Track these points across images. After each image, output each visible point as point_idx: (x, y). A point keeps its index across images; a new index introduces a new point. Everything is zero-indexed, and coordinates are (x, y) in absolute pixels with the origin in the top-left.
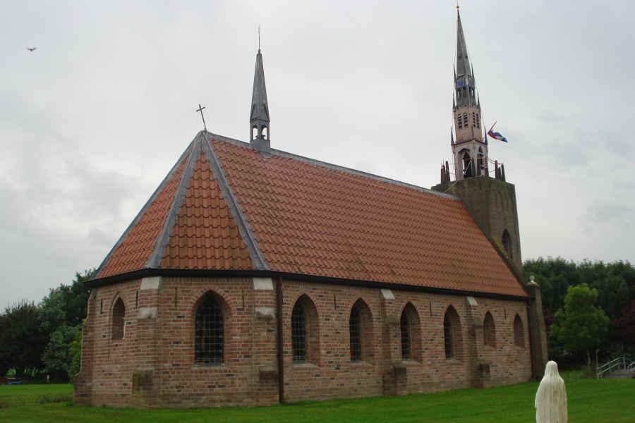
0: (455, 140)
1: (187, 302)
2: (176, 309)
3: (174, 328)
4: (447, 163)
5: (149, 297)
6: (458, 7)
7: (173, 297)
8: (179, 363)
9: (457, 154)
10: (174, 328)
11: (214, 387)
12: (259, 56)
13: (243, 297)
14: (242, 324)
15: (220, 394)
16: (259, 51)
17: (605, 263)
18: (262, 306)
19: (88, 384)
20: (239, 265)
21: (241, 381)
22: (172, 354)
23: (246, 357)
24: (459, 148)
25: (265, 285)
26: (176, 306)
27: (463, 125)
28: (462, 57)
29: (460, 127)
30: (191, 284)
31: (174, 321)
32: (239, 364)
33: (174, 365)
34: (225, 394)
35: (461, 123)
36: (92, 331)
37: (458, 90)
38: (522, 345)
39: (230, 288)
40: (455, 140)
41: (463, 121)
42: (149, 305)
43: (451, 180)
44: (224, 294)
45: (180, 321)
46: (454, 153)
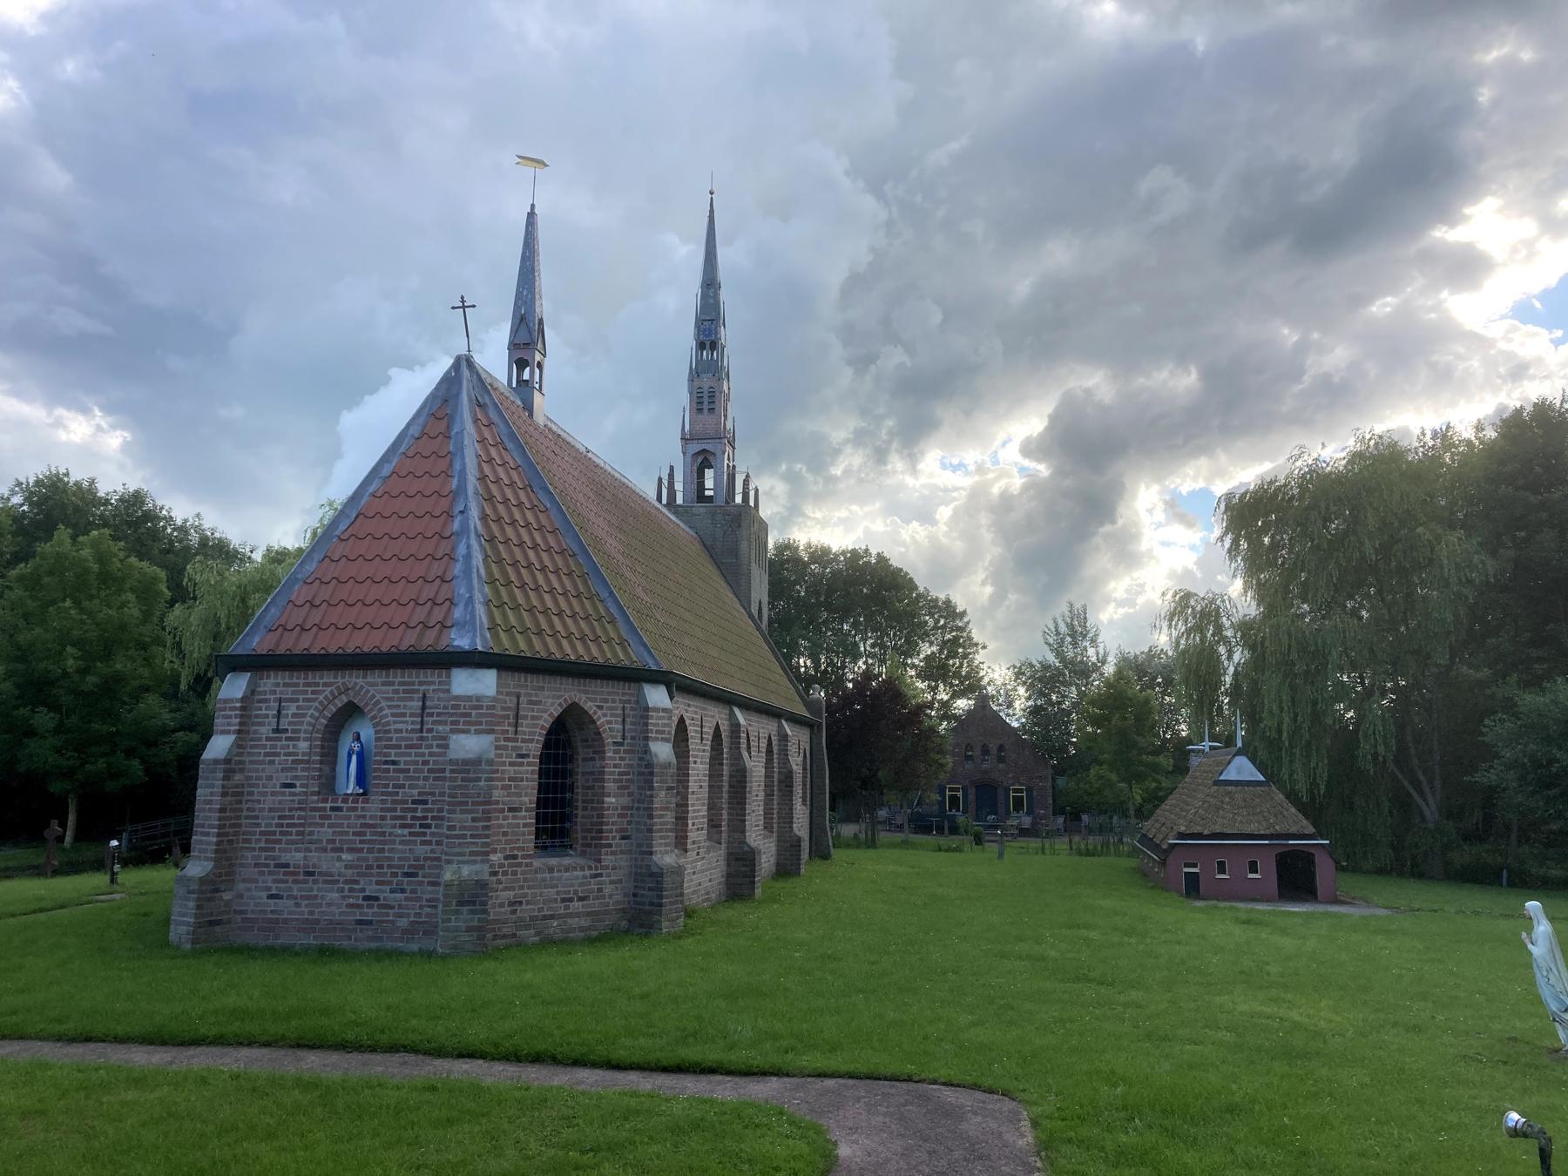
1: (535, 726)
2: (516, 740)
3: (510, 779)
5: (474, 712)
7: (512, 714)
8: (516, 852)
9: (689, 455)
10: (510, 779)
11: (571, 900)
13: (624, 720)
14: (620, 774)
15: (578, 915)
16: (533, 206)
19: (227, 896)
20: (619, 657)
21: (613, 886)
22: (505, 834)
23: (623, 838)
24: (695, 447)
25: (480, 684)
26: (516, 733)
29: (700, 410)
30: (542, 688)
31: (511, 764)
32: (613, 853)
33: (506, 858)
34: (589, 914)
36: (242, 770)
38: (805, 805)
39: (606, 701)
41: (706, 400)
42: (473, 728)
43: (678, 503)
44: (595, 713)
45: (522, 764)
46: (684, 453)
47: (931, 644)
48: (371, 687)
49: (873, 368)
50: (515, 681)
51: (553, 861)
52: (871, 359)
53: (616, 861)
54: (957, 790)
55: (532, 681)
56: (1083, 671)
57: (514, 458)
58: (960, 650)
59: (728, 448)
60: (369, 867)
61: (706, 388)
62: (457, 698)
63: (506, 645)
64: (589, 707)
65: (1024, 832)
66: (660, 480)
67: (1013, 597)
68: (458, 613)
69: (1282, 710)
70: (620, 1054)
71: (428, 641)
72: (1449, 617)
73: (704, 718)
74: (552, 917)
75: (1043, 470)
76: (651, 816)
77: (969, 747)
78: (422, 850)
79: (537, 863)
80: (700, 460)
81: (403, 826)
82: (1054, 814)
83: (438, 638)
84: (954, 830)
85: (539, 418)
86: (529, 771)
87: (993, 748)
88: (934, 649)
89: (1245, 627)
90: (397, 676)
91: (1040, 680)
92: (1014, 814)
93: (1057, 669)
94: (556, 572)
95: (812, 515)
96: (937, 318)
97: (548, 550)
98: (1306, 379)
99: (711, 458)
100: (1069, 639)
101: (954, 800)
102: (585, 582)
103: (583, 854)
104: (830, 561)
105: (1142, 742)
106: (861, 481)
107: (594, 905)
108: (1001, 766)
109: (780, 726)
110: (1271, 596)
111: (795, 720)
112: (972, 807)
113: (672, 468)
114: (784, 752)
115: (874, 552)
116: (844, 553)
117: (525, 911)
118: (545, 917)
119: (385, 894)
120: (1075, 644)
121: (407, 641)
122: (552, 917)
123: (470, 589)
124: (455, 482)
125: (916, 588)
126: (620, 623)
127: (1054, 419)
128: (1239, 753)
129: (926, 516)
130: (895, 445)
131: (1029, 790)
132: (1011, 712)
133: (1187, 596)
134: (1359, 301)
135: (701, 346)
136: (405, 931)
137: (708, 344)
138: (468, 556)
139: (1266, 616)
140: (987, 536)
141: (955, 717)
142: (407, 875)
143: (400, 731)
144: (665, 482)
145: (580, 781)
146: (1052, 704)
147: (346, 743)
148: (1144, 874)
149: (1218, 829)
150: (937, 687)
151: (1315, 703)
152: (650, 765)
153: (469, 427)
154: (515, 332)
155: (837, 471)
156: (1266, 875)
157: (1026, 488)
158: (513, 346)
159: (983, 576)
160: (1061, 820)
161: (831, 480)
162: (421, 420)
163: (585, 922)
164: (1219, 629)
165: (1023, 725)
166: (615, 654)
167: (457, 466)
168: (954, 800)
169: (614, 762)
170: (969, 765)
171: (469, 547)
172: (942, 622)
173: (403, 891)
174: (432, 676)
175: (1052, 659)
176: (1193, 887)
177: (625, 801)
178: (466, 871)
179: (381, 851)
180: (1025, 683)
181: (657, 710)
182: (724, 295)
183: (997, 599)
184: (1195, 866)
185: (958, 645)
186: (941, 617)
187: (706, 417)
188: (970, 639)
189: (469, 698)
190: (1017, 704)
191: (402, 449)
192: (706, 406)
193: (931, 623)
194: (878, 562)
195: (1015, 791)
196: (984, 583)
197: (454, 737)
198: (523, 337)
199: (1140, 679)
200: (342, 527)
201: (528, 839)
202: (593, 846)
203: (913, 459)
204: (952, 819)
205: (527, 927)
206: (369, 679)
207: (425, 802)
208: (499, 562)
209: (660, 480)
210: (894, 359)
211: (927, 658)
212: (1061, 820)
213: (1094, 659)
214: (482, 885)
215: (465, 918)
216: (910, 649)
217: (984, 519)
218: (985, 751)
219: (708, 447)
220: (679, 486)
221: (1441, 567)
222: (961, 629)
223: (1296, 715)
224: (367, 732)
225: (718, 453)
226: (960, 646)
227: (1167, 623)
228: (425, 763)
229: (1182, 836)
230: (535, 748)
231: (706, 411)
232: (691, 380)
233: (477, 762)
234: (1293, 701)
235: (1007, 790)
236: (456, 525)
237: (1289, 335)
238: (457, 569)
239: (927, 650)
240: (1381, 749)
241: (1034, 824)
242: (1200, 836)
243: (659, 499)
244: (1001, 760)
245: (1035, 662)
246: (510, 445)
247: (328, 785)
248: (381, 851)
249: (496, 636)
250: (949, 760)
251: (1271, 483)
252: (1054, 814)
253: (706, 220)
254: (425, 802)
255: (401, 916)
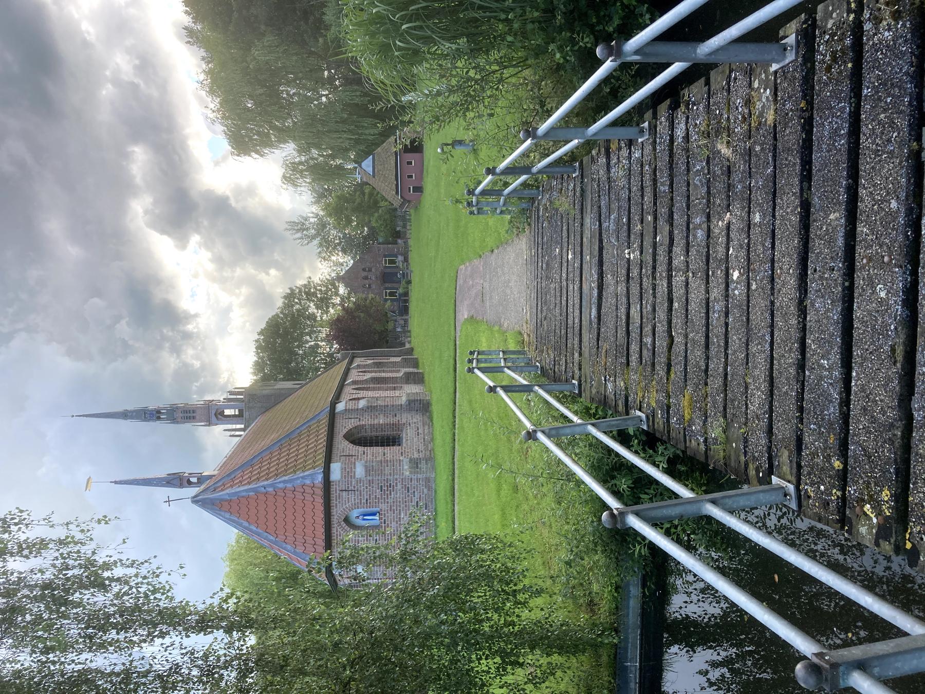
9: (217, 422)
15: (424, 430)
16: (111, 482)
20: (325, 422)
24: (214, 419)
29: (194, 418)
31: (367, 456)
34: (424, 426)
47: (309, 306)
48: (337, 513)
49: (131, 342)
50: (334, 457)
51: (404, 440)
52: (125, 344)
53: (405, 418)
54: (386, 292)
55: (335, 451)
56: (322, 225)
57: (239, 474)
58: (312, 290)
59: (214, 403)
60: (406, 506)
61: (181, 415)
62: (342, 477)
63: (321, 461)
64: (345, 431)
65: (406, 260)
66: (231, 436)
67: (277, 256)
68: (308, 482)
69: (340, 138)
70: (452, 390)
71: (320, 492)
72: (295, 58)
73: (348, 391)
74: (424, 439)
75: (195, 239)
76: (387, 406)
77: (364, 286)
78: (399, 486)
79: (404, 445)
80: (220, 417)
81: (391, 494)
82: (396, 244)
83: (318, 488)
84: (406, 294)
85: (216, 473)
86: (369, 450)
87: (365, 274)
88: (312, 305)
89: (301, 150)
90: (333, 502)
91: (328, 248)
92: (397, 264)
93: (321, 239)
94: (289, 450)
95: (226, 379)
96: (96, 300)
97: (280, 454)
98: (136, 81)
99: (219, 411)
100: (305, 232)
101: (392, 294)
102: (294, 439)
103: (402, 431)
104: (263, 362)
105: (358, 200)
106: (203, 349)
107: (420, 425)
108: (373, 270)
109: (353, 368)
110: (284, 135)
111: (351, 362)
112: (395, 285)
113: (225, 430)
114: (365, 366)
115: (257, 337)
116: (258, 353)
117: (422, 448)
118: (424, 441)
119: (415, 499)
120: (307, 229)
121: (320, 500)
122: (424, 439)
123: (298, 478)
124: (251, 494)
125: (277, 315)
126: (311, 423)
127: (163, 232)
128: (360, 166)
129: (226, 312)
130: (181, 328)
131: (385, 256)
132: (345, 264)
133: (284, 177)
134: (86, 44)
135: (159, 418)
136: (429, 490)
137: (158, 415)
138: (284, 482)
139: (294, 139)
140: (239, 272)
141: (349, 294)
142: (408, 491)
143: (355, 499)
144: (233, 433)
145: (374, 434)
146: (341, 242)
147: (359, 522)
148: (416, 208)
149: (394, 177)
150: (332, 303)
151: (337, 122)
152: (368, 408)
153: (227, 491)
154: (174, 486)
155: (197, 364)
156: (412, 157)
157: (208, 248)
158: (181, 486)
159: (264, 274)
160: (399, 241)
161: (203, 367)
162: (223, 513)
163: (426, 427)
164: (301, 163)
165: (352, 258)
166: (323, 437)
167: (244, 494)
168: (392, 294)
169: (367, 421)
170: (373, 286)
171: (280, 482)
172: (296, 300)
173: (414, 492)
174: (333, 488)
175: (316, 242)
176: (419, 189)
177: (382, 416)
178: (406, 467)
179: (400, 502)
180: (329, 256)
181: (346, 406)
182: (130, 407)
183: (278, 266)
184: (410, 188)
185: (308, 292)
186: (294, 301)
187: (197, 415)
188: (305, 286)
189: (342, 472)
190: (341, 261)
191: (236, 519)
192: (192, 415)
193: (298, 306)
194: (264, 335)
195: (386, 263)
196: (268, 274)
197: (357, 477)
198: (177, 482)
199: (326, 196)
200: (272, 538)
201: (396, 449)
202: (398, 427)
203: (188, 317)
204: (400, 295)
205: (427, 446)
206: (335, 513)
207: (381, 486)
208: (286, 470)
209: (231, 436)
210: (124, 329)
211: (317, 308)
212: (399, 241)
213: (316, 219)
214: (411, 460)
215: (423, 465)
216: (312, 317)
217: (227, 273)
218: (366, 278)
219: (214, 412)
220: (234, 426)
221: (270, 60)
222: (300, 291)
223: (343, 131)
224: (355, 513)
225: (217, 407)
226: (310, 291)
227: (299, 188)
228: (367, 488)
229: (397, 193)
230: (361, 449)
231: (194, 415)
232: (178, 423)
233: (366, 467)
234: (336, 132)
235: (386, 267)
236: (270, 489)
237: (107, 91)
238: (289, 485)
239: (312, 309)
240: (358, 93)
241: (402, 255)
242: (397, 185)
243: (240, 436)
244: (370, 270)
245: (318, 250)
246: (233, 476)
247: (374, 527)
248: (400, 502)
249: (317, 466)
250: (371, 296)
251: (225, 134)
252: (396, 244)
253: (88, 418)
254: (381, 486)
255: (423, 492)
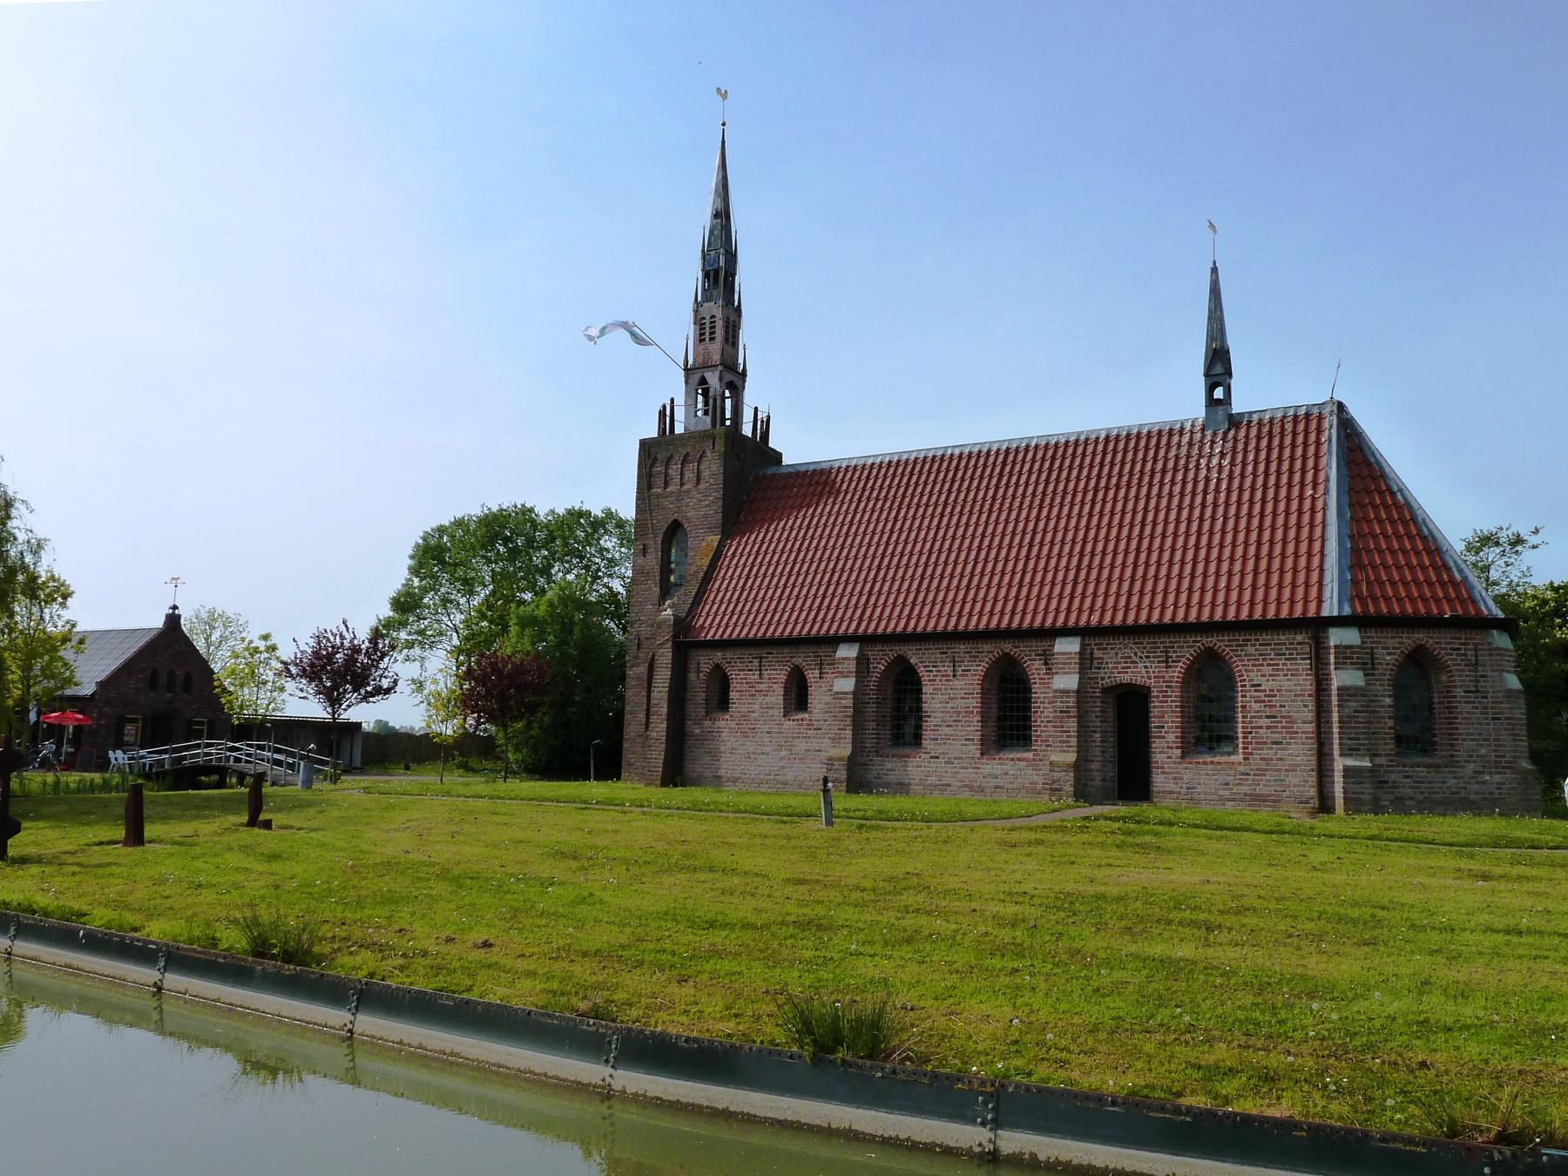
0: (691, 362)
4: (672, 400)
6: (724, 124)
12: (1214, 270)
16: (1214, 263)
17: (542, 512)
18: (1346, 663)
27: (707, 336)
28: (722, 216)
29: (702, 340)
35: (711, 328)
37: (706, 275)
40: (691, 362)
